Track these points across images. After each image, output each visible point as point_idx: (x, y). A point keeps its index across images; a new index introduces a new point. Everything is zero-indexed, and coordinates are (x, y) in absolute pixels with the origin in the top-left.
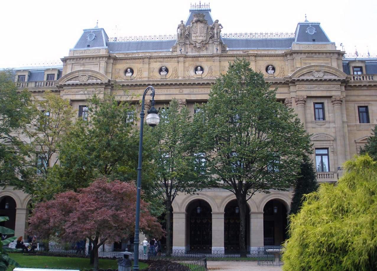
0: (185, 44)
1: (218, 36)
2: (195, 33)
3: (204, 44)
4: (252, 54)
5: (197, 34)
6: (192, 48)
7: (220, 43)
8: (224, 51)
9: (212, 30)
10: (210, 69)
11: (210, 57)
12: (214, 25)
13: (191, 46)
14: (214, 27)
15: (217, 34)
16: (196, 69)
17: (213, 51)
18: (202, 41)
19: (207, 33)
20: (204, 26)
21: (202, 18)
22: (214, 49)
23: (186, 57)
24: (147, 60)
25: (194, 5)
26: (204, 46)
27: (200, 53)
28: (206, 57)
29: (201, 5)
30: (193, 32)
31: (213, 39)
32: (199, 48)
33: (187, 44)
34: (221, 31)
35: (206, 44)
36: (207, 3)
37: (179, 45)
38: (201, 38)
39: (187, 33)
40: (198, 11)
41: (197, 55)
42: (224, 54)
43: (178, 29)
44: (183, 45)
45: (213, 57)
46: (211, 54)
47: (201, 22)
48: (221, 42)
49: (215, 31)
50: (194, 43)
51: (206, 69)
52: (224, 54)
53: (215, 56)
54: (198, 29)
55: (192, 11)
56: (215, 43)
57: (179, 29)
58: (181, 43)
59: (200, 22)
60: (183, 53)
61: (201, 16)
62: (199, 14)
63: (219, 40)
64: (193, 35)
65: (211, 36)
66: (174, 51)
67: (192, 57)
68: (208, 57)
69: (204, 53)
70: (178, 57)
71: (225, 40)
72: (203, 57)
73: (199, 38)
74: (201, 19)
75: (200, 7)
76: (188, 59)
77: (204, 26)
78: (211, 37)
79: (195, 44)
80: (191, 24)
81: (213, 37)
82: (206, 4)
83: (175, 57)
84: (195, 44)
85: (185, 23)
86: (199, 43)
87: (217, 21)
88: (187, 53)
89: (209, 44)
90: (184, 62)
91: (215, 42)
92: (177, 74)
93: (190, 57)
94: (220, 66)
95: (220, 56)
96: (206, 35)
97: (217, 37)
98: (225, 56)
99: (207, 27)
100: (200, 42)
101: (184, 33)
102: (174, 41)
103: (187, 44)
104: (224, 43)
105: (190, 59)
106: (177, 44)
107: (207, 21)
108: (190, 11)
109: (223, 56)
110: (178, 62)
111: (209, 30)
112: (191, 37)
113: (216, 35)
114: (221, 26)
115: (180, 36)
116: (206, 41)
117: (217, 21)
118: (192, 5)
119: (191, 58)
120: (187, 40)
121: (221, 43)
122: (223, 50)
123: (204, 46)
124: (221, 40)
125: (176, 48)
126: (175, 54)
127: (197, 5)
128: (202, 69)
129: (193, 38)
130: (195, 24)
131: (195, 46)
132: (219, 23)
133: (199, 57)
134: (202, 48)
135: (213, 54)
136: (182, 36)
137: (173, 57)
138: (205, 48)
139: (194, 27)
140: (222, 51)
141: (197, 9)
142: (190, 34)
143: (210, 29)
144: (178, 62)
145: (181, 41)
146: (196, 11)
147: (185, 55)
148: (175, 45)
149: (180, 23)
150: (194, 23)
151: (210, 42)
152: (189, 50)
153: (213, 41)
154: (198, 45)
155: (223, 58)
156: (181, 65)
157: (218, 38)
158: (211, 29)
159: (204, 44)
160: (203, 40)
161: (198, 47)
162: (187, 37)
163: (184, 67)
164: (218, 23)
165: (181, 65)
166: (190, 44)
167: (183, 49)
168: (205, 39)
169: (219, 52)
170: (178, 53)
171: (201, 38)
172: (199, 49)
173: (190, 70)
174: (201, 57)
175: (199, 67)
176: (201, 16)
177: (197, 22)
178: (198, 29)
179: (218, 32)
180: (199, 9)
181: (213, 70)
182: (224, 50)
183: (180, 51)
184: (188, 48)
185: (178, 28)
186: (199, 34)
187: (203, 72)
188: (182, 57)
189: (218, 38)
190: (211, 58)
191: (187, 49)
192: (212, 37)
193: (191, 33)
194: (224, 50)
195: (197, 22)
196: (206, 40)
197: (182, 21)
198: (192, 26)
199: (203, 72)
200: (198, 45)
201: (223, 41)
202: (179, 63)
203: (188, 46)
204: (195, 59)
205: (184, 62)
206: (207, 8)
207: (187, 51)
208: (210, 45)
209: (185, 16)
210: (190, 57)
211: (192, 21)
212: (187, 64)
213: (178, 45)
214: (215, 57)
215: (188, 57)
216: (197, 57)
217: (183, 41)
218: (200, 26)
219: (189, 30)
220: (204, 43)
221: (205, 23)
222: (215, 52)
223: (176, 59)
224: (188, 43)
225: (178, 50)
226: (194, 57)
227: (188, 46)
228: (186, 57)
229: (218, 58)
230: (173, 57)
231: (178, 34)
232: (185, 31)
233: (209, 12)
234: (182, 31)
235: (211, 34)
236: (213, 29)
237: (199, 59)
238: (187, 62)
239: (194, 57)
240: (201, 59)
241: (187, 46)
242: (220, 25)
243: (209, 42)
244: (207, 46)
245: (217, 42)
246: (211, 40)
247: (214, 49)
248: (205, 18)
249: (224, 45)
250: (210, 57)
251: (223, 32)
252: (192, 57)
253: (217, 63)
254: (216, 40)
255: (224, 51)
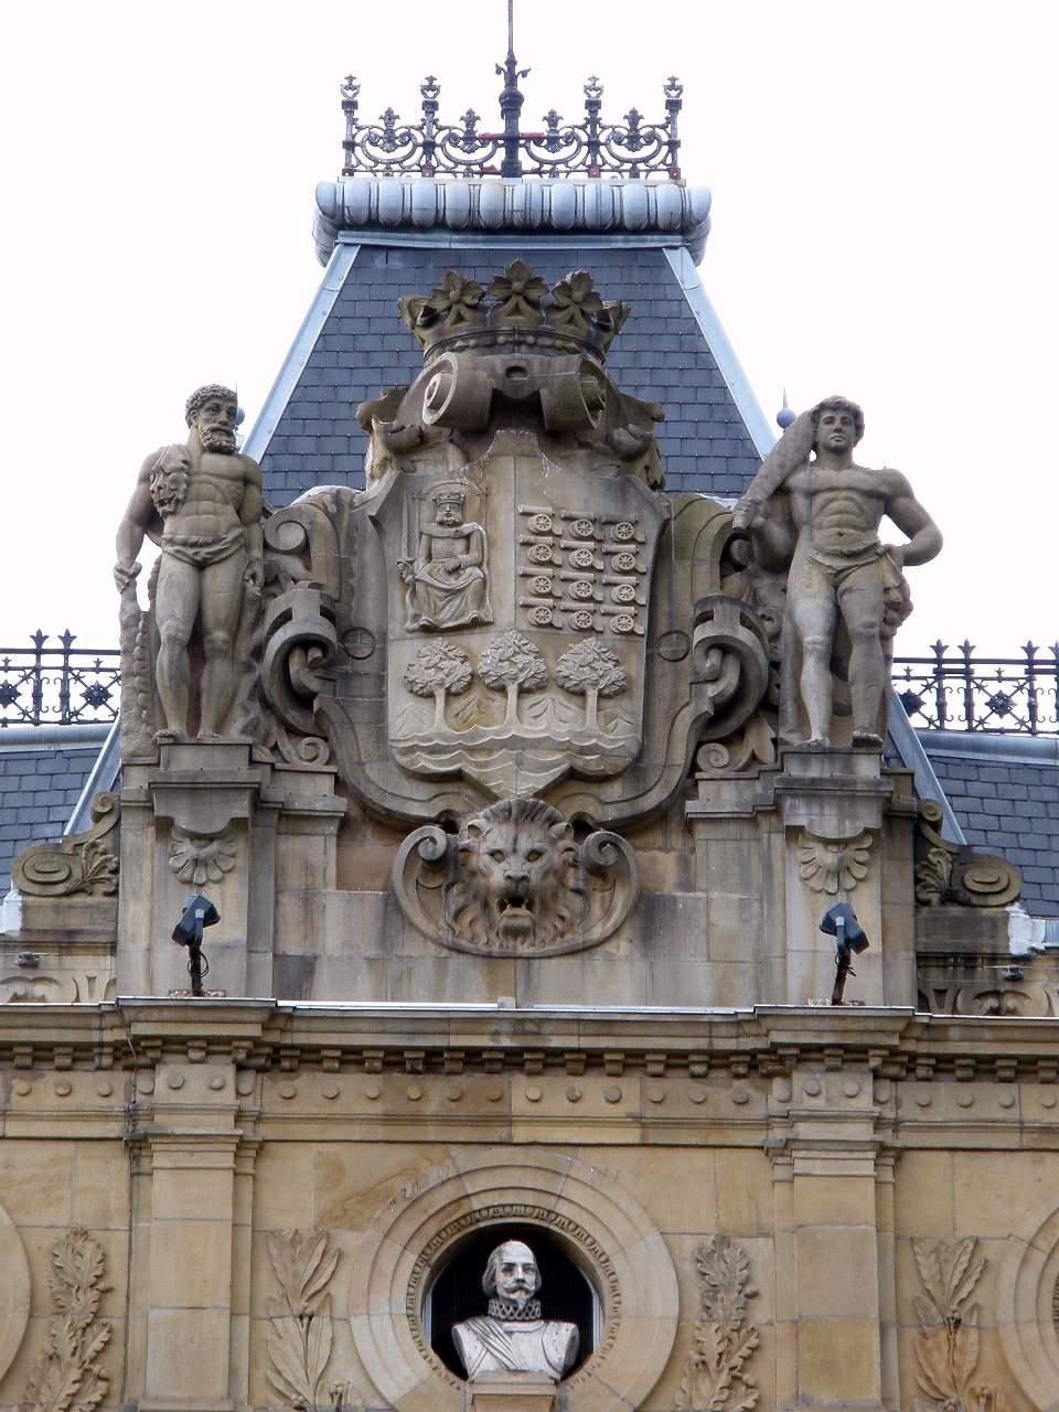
0: (268, 817)
1: (859, 694)
2: (446, 618)
3: (610, 833)
4: (381, 1021)
5: (488, 652)
6: (391, 904)
7: (890, 816)
8: (969, 960)
9: (763, 572)
10: (719, 1280)
11: (717, 1060)
12: (782, 491)
13: (372, 849)
14: (777, 533)
15: (836, 664)
16: (457, 1290)
17: (762, 962)
18: (572, 775)
19: (658, 639)
20: (603, 506)
21: (564, 368)
22: (776, 928)
23: (275, 1051)
24: (195, 1092)
25: (411, 115)
26: (598, 872)
27: (530, 989)
28: (633, 1061)
29: (531, 121)
30: (401, 614)
31: (760, 740)
32: (516, 896)
33: (294, 820)
34: (897, 608)
35: (632, 827)
36: (632, 95)
37: (164, 827)
38: (551, 720)
39: (307, 620)
40: (472, 225)
41: (477, 1021)
42: (966, 1025)
43: (135, 548)
44: (238, 824)
45: (767, 1063)
46: (737, 1022)
47: (560, 433)
48: (905, 800)
49: (806, 603)
50: (417, 802)
51: (644, 1294)
52: (966, 1025)
53: (807, 1053)
54: (507, 562)
55: (372, 223)
56: (800, 814)
57: (150, 552)
58: (193, 789)
59: (529, 439)
60: (226, 980)
61: (521, 314)
62: (519, 288)
63: (867, 768)
64: (408, 657)
65: (730, 681)
66: (67, 942)
67: (393, 1060)
68: (676, 1061)
69: (606, 989)
70: (137, 1055)
71: (961, 758)
72: (592, 1061)
73: (509, 719)
74: (555, 373)
75: (511, 169)
76: (311, 1090)
77: (603, 506)
78: (724, 709)
79: (449, 824)
80: (374, 452)
81: (769, 708)
82: (613, 115)
83: (81, 1054)
84: (449, 824)
85: (252, 436)
86: (526, 813)
87: (836, 425)
88: (298, 974)
89: (689, 826)
90: (250, 1150)
91: (812, 791)
92: (111, 1365)
93: (351, 1058)
94: (896, 1238)
95: (900, 1059)
96: (636, 668)
97: (840, 710)
98: (983, 1068)
99: (649, 532)
100: (522, 785)
101: (248, 611)
102: (67, 754)
103: (294, 820)
104: (953, 832)
105: (357, 1091)
106: (112, 812)
107: (647, 414)
108: (338, 221)
109: (944, 1065)
110: (136, 1146)
111: (698, 578)
112: (366, 686)
113: (813, 678)
114: (912, 522)
115: (184, 661)
116: (635, 768)
117: (836, 425)
118: (369, 115)
119: (371, 1084)
120: (297, 752)
121: (907, 825)
122: (943, 942)
123: (598, 872)
124: (897, 772)
125: (96, 877)
126: (78, 984)
127: (450, 115)
128: (566, 1289)
129: (409, 720)
130: (444, 472)
131: (446, 868)
132: (868, 455)
133: (513, 1060)
134: (570, 905)
135: (758, 1018)
136: (218, 673)
137: (42, 1054)
138: (621, 899)
139: (426, 518)
140: (923, 960)
141: (452, 190)
142: (348, 632)
143: (706, 554)
144: (136, 1146)
145: (186, 762)
146: (439, 224)
147: (274, 1013)
148: (77, 820)
149: (176, 433)
150: (422, 441)
151: (719, 796)
152: (340, 925)
153: (759, 790)
154: (497, 850)
155: (947, 1099)
156: (189, 1196)
157: (862, 722)
158: (728, 564)
159: (610, 833)
160: (591, 763)
161: (498, 875)
162: (303, 700)
163: (251, 1236)
164: (841, 454)
165: (189, 1196)
166: (345, 825)
167: (229, 898)
168: (617, 734)
169: (880, 987)
170: (147, 970)
171: (552, 722)
172: (522, 916)
173: (339, 1291)
174: (553, 1060)
175: (517, 1252)
176: (521, 314)
177: (476, 423)
178: (507, 562)
179: (860, 614)
180: (490, 193)
181: (760, 1313)
182: (956, 959)
183: (187, 936)
184: (309, 900)
185: (147, 519)
186: (505, 643)
187: (582, 1350)
188: (212, 1047)
189: (862, 722)
190: (722, 1095)
191: (291, 908)
192: (742, 711)
193: (371, 620)
194: (956, 959)
195: (476, 423)
196: (639, 758)
197: (215, 408)
198: (394, 498)
199: (582, 1350)
200: (498, 836)
201: (931, 789)
202: (161, 1158)
203: (319, 848)
204: (437, 1093)
205: (250, 1150)
206: (632, 194)
207: (293, 946)
208: (713, 850)
209: (258, 320)
210: (351, 1058)
211: (389, 408)
212: (295, 1190)
213: (137, 837)
214: (802, 1080)
215: (310, 1057)
216: (473, 1059)
217: (234, 767)
218: (530, 491)
219: (343, 569)
220: (609, 803)
221: (631, 457)
222: (804, 972)
223: (91, 1088)
224: (316, 794)
225: (144, 911)
226: (433, 1061)
227: (319, 848)
228: (275, 1051)
229: (854, 1093)
230: (42, 1054)
231: (140, 628)
232: (273, 581)
233: (677, 260)
234: (221, 581)
235: (723, 647)
236: (755, 556)
237: (522, 1091)
238: (304, 1158)
239: (433, 1061)
240: (557, 1104)
241: (292, 846)
242: (890, 497)
243: (689, 784)
244: (660, 862)
245: (843, 793)
246: (717, 757)
247: (776, 928)
248: (626, 367)
249: (963, 857)
250: (717, 1060)
251: (943, 610)
252: (393, 1060)
253: (838, 1191)
254: (815, 770)
255: (969, 960)
